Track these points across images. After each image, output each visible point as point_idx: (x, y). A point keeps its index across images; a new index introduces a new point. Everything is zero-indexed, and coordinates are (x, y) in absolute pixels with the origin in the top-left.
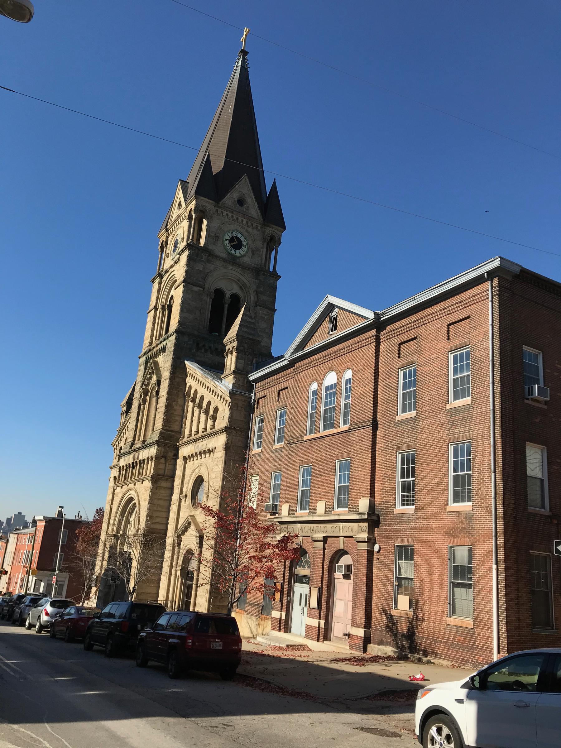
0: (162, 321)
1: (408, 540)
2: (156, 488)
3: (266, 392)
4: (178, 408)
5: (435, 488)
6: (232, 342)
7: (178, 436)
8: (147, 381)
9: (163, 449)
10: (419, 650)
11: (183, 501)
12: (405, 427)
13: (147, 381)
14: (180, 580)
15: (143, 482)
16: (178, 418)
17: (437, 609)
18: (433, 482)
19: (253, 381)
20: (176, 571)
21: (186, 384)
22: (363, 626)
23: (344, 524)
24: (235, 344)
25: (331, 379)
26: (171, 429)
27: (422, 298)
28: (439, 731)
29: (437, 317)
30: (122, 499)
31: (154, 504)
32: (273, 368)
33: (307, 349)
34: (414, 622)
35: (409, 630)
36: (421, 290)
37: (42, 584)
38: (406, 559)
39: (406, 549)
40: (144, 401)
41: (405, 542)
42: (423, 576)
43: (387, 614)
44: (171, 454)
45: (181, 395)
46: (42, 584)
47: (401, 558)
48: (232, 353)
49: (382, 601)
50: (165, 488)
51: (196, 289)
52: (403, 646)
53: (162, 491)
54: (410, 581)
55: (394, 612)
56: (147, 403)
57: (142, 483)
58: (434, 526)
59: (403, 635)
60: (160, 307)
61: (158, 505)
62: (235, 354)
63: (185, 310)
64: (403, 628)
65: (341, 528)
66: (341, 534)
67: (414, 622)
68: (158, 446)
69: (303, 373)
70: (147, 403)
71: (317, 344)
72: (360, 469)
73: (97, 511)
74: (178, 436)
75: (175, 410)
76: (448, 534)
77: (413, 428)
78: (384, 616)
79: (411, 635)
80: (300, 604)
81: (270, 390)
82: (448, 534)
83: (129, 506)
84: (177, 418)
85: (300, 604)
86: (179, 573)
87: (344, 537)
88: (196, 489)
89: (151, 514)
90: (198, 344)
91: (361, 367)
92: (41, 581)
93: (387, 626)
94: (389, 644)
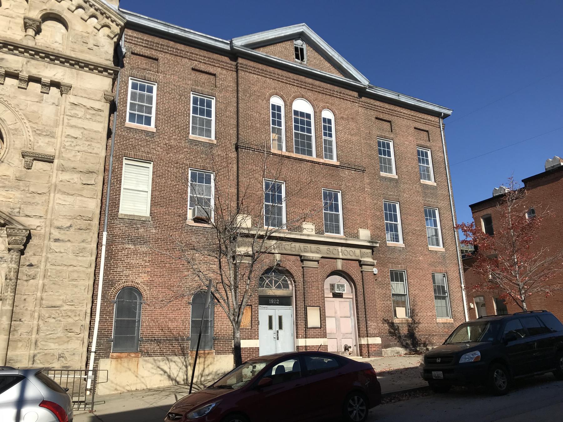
1: (401, 267)
3: (160, 55)
5: (418, 233)
10: (420, 344)
12: (389, 183)
17: (429, 314)
18: (416, 228)
23: (344, 248)
25: (302, 106)
27: (403, 99)
28: (353, 400)
32: (192, 37)
33: (254, 52)
34: (412, 327)
35: (409, 331)
36: (405, 94)
38: (397, 280)
39: (396, 274)
41: (398, 268)
42: (416, 292)
43: (388, 323)
47: (392, 280)
49: (383, 314)
52: (407, 344)
54: (403, 297)
55: (396, 321)
58: (420, 259)
59: (406, 336)
64: (404, 331)
65: (340, 251)
66: (341, 256)
67: (412, 327)
69: (254, 76)
71: (276, 57)
72: (355, 204)
76: (431, 265)
77: (396, 187)
78: (386, 325)
79: (411, 335)
80: (271, 327)
81: (168, 56)
82: (431, 265)
83: (131, 79)
85: (271, 327)
87: (343, 259)
91: (345, 116)
93: (390, 332)
94: (395, 345)
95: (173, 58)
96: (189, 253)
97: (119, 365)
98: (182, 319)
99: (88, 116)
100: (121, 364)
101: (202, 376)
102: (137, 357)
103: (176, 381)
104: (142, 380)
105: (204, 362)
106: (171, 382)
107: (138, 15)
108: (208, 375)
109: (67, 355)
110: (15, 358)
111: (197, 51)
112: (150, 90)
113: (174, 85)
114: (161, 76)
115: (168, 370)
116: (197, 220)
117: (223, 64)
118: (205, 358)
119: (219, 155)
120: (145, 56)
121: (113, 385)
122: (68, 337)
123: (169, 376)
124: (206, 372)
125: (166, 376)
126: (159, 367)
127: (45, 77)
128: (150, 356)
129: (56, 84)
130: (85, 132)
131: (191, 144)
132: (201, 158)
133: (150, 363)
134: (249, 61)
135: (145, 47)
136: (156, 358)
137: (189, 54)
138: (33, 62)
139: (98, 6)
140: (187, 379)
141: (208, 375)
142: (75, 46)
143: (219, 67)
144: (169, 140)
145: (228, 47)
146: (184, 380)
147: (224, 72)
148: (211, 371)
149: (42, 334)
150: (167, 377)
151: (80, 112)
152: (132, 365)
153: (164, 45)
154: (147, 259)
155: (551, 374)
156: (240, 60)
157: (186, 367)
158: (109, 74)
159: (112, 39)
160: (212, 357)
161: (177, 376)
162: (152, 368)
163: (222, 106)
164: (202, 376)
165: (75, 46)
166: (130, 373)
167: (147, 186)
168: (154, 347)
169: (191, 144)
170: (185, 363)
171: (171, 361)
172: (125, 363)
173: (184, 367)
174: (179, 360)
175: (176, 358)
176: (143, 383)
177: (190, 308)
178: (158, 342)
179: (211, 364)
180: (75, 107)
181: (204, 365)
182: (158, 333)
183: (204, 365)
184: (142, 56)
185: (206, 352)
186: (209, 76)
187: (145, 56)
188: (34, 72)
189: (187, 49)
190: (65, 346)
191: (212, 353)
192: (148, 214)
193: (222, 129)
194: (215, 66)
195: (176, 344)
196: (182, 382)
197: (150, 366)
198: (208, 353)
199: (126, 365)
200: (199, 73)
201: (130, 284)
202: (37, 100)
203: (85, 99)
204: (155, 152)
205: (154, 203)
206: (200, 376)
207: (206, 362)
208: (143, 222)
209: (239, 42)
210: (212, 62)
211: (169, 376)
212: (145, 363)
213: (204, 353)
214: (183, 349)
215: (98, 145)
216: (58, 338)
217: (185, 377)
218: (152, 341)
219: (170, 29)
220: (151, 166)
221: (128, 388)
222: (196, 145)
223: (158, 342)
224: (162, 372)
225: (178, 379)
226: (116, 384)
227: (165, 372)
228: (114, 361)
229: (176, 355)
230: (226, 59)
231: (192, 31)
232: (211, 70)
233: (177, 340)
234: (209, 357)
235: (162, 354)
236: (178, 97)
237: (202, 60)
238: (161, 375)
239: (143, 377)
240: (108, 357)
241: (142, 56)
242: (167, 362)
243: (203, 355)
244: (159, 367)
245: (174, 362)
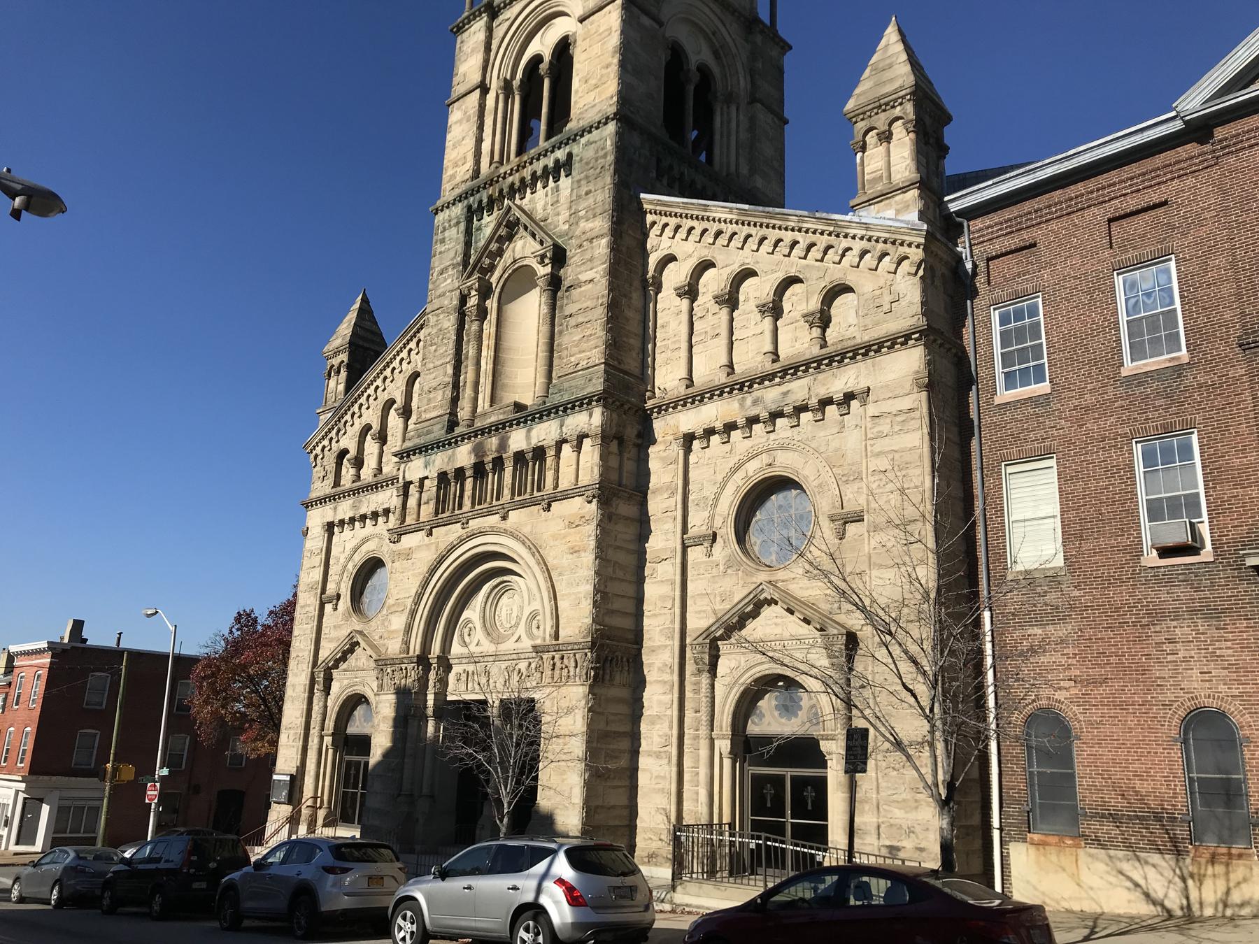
0: (505, 118)
2: (610, 519)
3: (1036, 234)
4: (633, 316)
6: (336, 354)
7: (642, 388)
8: (487, 261)
9: (615, 416)
11: (328, 607)
13: (487, 261)
14: (330, 752)
15: (549, 505)
16: (635, 342)
19: (960, 213)
20: (322, 738)
21: (645, 255)
22: (25, 765)
24: (344, 357)
26: (622, 367)
29: (1182, 165)
30: (440, 562)
31: (609, 561)
37: (45, 809)
40: (482, 313)
44: (631, 432)
45: (637, 283)
46: (45, 809)
48: (338, 372)
50: (627, 519)
51: (646, 21)
53: (620, 527)
56: (492, 316)
57: (548, 508)
60: (495, 84)
61: (615, 563)
62: (343, 374)
63: (629, 67)
68: (604, 407)
70: (492, 316)
73: (238, 619)
74: (642, 388)
75: (627, 320)
81: (1054, 225)
84: (632, 341)
86: (328, 740)
88: (743, 517)
89: (602, 588)
90: (659, 161)
92: (41, 801)
95: (1064, 222)
96: (1158, 628)
97: (1042, 858)
98: (1164, 776)
99: (897, 428)
100: (1045, 856)
101: (1226, 906)
102: (1078, 846)
103: (1163, 906)
104: (1091, 893)
105: (1227, 873)
106: (1152, 907)
107: (975, 188)
108: (1242, 905)
109: (918, 829)
110: (863, 827)
111: (1114, 176)
112: (1033, 312)
113: (1075, 278)
114: (1046, 274)
115: (1142, 882)
116: (1165, 552)
117: (1182, 165)
118: (1227, 865)
119: (1200, 386)
120: (1011, 252)
121: (1037, 893)
122: (916, 801)
123: (1147, 895)
124: (1236, 897)
125: (1138, 894)
126: (1121, 873)
127: (836, 392)
128: (1103, 847)
129: (849, 397)
130: (897, 456)
131: (1129, 386)
132: (1156, 408)
133: (1102, 861)
134: (1244, 120)
135: (1008, 234)
136: (1112, 853)
137: (1095, 195)
138: (820, 376)
139: (884, 235)
140: (1189, 906)
141: (1242, 905)
142: (868, 321)
143: (1173, 179)
144: (1082, 395)
145: (1178, 125)
146: (1182, 908)
147: (1190, 181)
148: (1247, 897)
149: (882, 794)
150: (1143, 897)
151: (884, 426)
152: (1066, 860)
153: (1040, 210)
154: (1070, 651)
155: (196, 885)
156: (1219, 133)
157: (1184, 880)
158: (916, 340)
159: (916, 273)
160: (1245, 865)
161: (1166, 896)
162: (1108, 873)
163: (1194, 267)
164: (1226, 906)
165: (868, 321)
166: (1064, 875)
167: (1052, 506)
168: (1107, 829)
169: (1129, 386)
170: (1178, 871)
171: (1147, 863)
172: (1053, 855)
173: (1177, 879)
174: (1164, 864)
175: (1155, 858)
176: (1093, 899)
177: (1177, 754)
178: (1115, 818)
179: (1245, 880)
180: (877, 420)
181: (1228, 880)
182: (1115, 802)
183: (1228, 880)
184: (1007, 253)
185: (1234, 851)
186: (1153, 213)
187: (1011, 252)
188: (823, 392)
189: (1092, 184)
190: (912, 816)
191: (1250, 855)
192: (1059, 562)
193: (1202, 320)
194: (1163, 183)
195: (1155, 827)
196: (1179, 913)
197: (1101, 867)
198: (1240, 856)
199: (1054, 858)
200: (1129, 220)
201: (1044, 702)
202: (836, 430)
203: (890, 401)
204: (1055, 433)
205: (1070, 535)
206: (1220, 907)
207: (1232, 876)
208: (1054, 579)
209: (1193, 102)
210: (1153, 178)
211: (1147, 895)
212: (1090, 860)
213: (1230, 855)
214: (1173, 840)
215: (918, 471)
216: (904, 800)
217: (1185, 902)
218: (1103, 816)
219: (1038, 174)
220: (1052, 462)
221: (1066, 905)
222: (1140, 384)
223: (1115, 818)
224: (1129, 884)
225: (1167, 904)
226: (1043, 893)
227: (1137, 885)
228: (1032, 849)
229: (1160, 851)
230: (1192, 149)
231: (1081, 148)
232: (1155, 198)
233: (1158, 818)
234: (1238, 865)
235: (1129, 847)
236: (1085, 298)
237: (1124, 188)
238: (1129, 889)
239: (1091, 888)
240: (1024, 840)
241: (1007, 253)
242: (1137, 864)
243: (1225, 859)
244: (1121, 873)
245: (1154, 866)
